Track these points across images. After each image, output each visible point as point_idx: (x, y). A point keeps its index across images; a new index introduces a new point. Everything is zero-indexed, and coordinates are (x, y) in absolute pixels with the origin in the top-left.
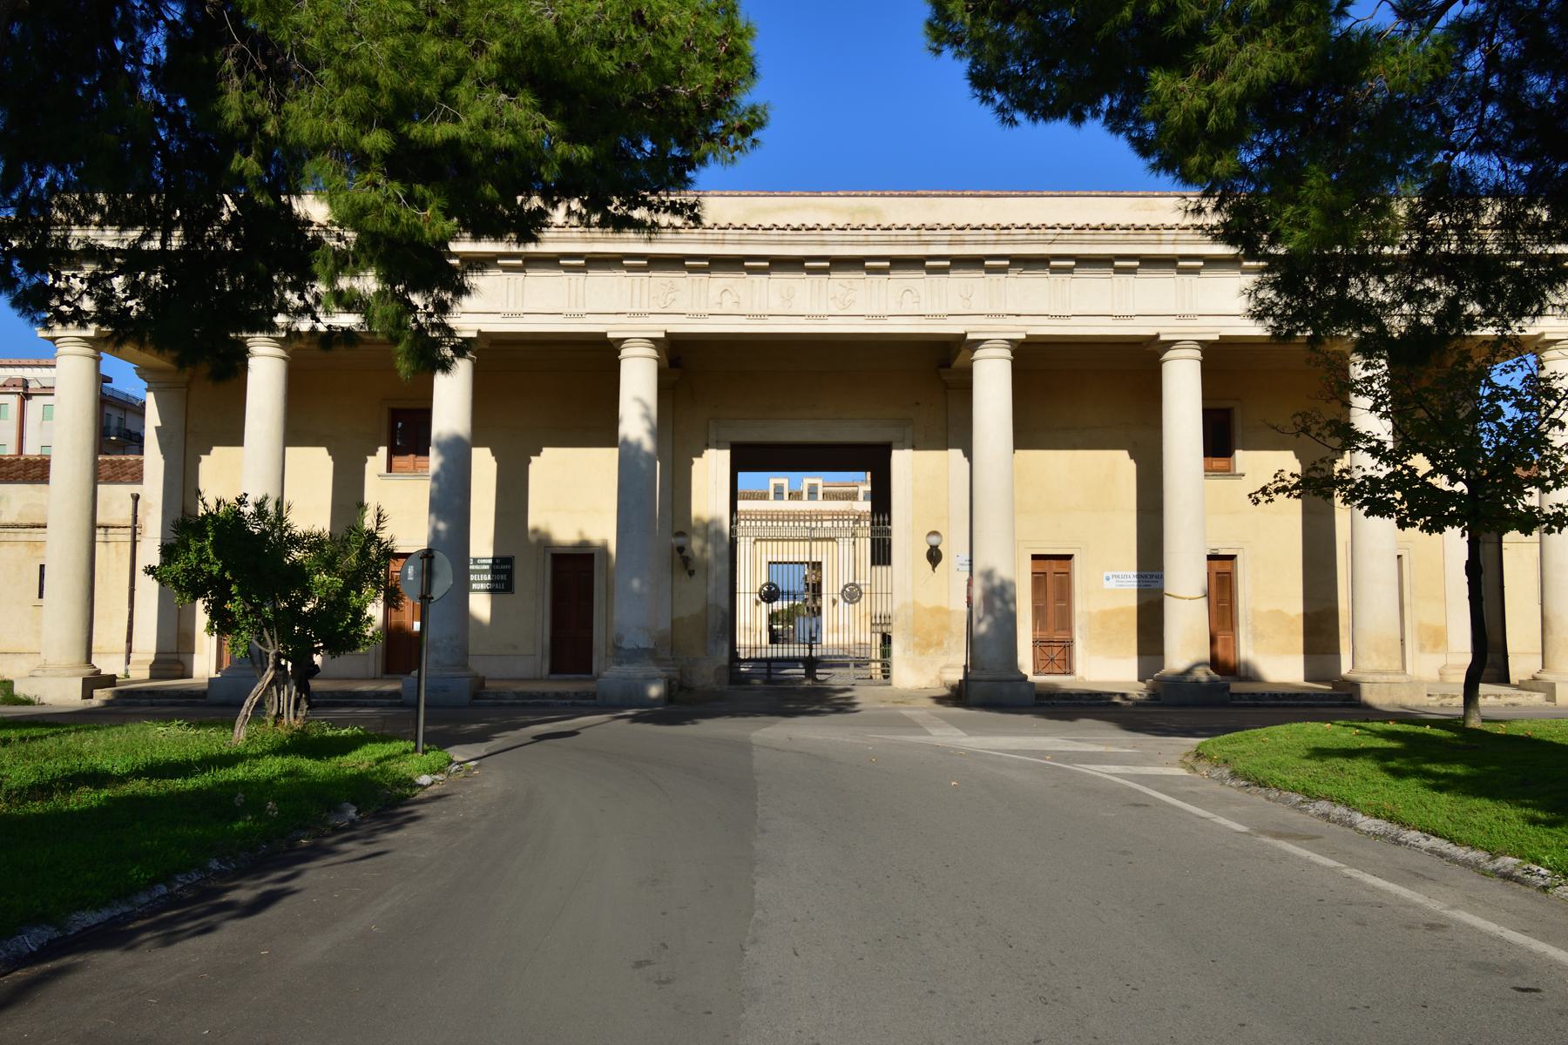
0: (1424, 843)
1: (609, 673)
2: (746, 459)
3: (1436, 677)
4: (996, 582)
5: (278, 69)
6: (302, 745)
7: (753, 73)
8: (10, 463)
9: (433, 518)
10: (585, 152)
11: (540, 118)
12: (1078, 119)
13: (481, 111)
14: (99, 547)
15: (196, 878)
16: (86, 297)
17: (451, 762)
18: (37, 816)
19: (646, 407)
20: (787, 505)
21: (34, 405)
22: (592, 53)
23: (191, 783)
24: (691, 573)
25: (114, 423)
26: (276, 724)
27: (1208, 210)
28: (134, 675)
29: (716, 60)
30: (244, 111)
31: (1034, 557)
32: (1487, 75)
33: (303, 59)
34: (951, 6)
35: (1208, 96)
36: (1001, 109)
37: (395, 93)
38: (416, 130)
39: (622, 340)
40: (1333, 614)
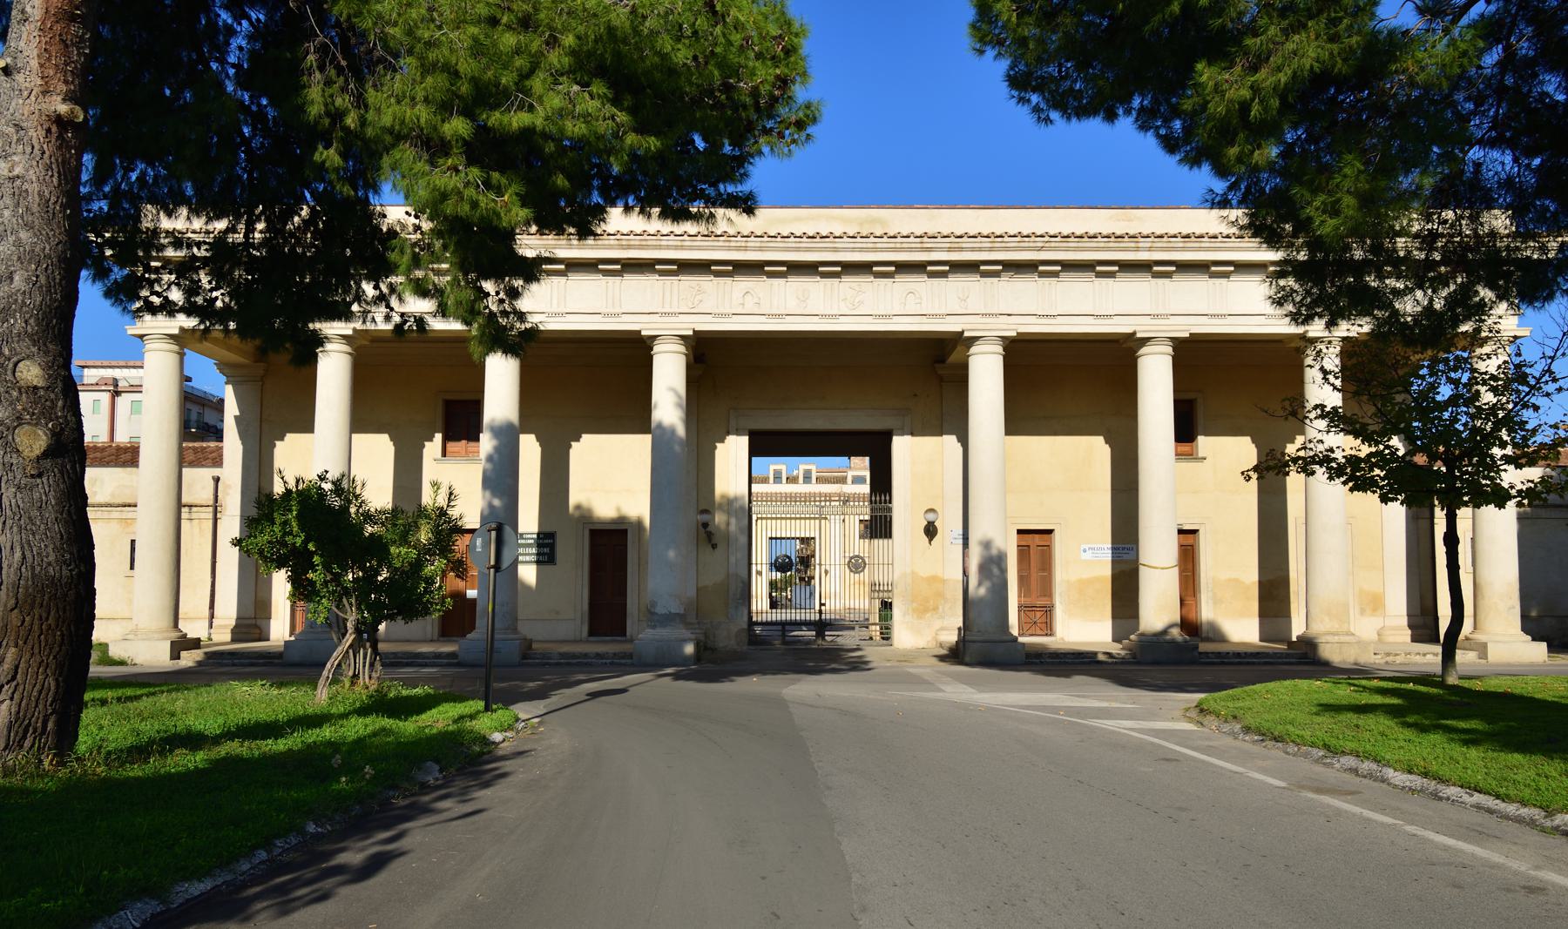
0: (1466, 798)
1: (643, 635)
2: (762, 445)
3: (1375, 637)
4: (994, 552)
5: (361, 60)
6: (380, 705)
7: (804, 74)
8: (103, 449)
9: (488, 494)
10: (653, 143)
11: (609, 109)
12: (1111, 117)
13: (556, 101)
14: (184, 523)
15: (294, 841)
16: (174, 288)
17: (517, 720)
18: (137, 779)
19: (679, 397)
20: (800, 488)
21: (123, 402)
22: (666, 43)
23: (281, 745)
24: (714, 546)
25: (194, 417)
26: (353, 684)
27: (1234, 202)
28: (216, 638)
29: (773, 58)
30: (326, 105)
31: (1020, 532)
32: (1503, 73)
33: (386, 47)
34: (999, 6)
35: (1252, 87)
36: (1036, 109)
37: (474, 81)
38: (495, 118)
39: (654, 337)
40: (1284, 582)
